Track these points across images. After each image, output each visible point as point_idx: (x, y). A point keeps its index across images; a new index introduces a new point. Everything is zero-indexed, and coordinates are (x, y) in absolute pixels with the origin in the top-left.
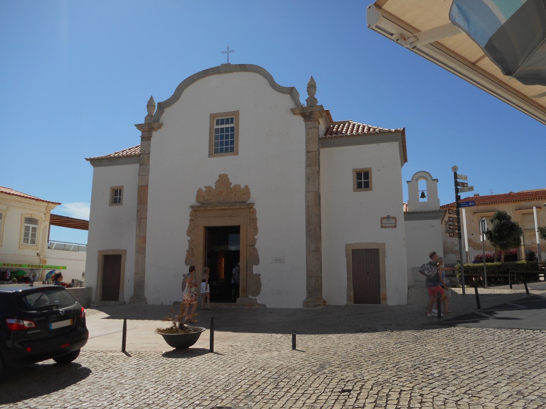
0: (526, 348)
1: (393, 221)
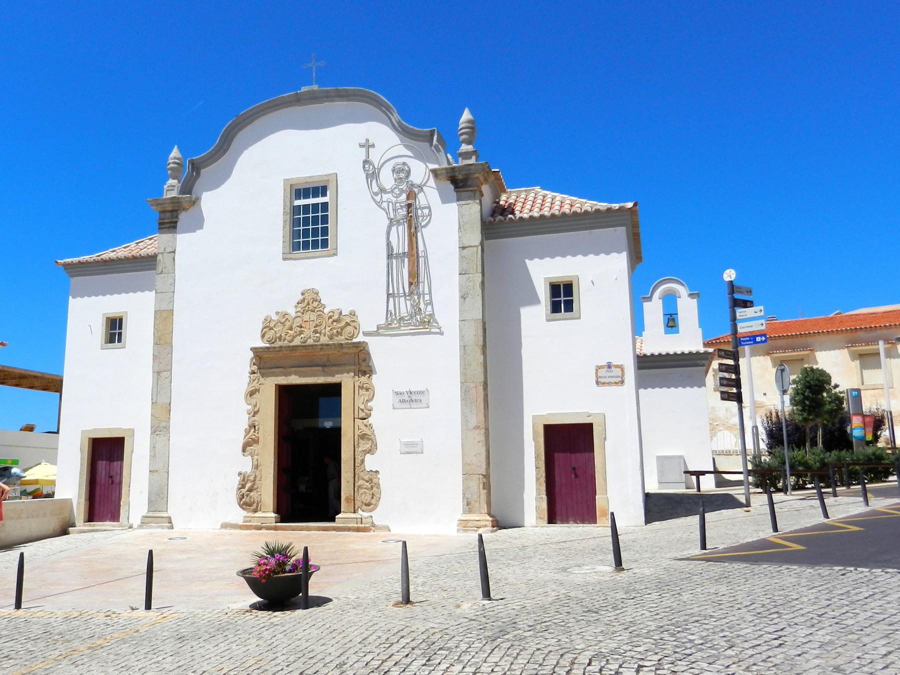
0: (856, 598)
1: (618, 372)
